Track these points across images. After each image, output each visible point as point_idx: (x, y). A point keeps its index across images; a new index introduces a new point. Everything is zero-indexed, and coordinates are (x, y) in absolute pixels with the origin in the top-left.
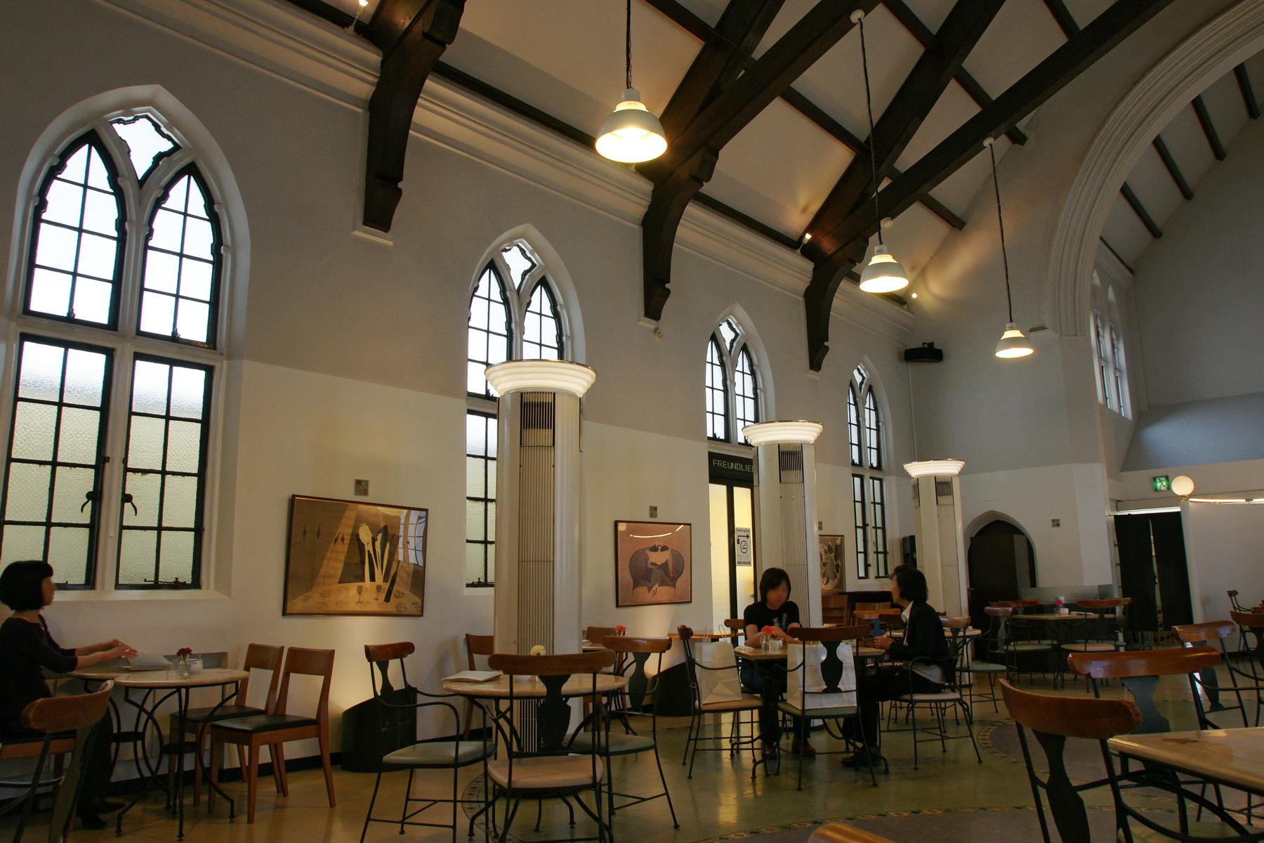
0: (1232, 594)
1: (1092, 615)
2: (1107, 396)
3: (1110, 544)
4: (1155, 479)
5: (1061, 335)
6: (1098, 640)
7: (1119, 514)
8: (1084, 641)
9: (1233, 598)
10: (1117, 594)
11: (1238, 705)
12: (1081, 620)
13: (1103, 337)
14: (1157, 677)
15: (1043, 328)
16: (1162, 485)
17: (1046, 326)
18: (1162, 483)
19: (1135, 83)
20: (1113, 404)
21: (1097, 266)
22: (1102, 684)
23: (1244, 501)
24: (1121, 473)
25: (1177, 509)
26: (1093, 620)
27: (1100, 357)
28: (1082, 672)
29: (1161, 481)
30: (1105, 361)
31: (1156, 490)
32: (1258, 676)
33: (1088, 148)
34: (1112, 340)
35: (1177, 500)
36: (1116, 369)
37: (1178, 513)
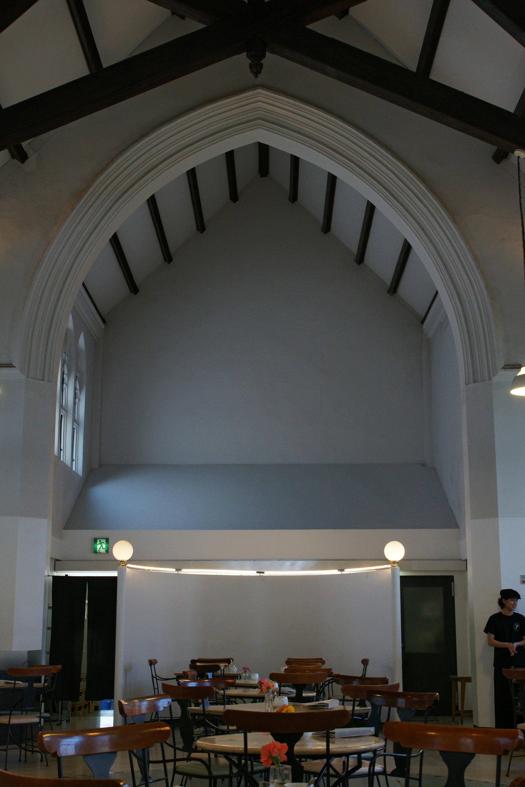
0: (152, 663)
1: (20, 684)
2: (62, 448)
3: (44, 607)
4: (95, 540)
5: (28, 377)
6: (22, 711)
7: (56, 574)
8: (9, 712)
9: (153, 666)
10: (44, 661)
11: (418, 777)
12: (9, 689)
13: (67, 385)
14: (115, 753)
15: (10, 366)
16: (101, 547)
17: (14, 365)
18: (102, 545)
19: (144, 135)
20: (66, 457)
21: (75, 313)
22: (20, 760)
23: (174, 570)
24: (64, 531)
25: (113, 574)
26: (21, 690)
27: (61, 406)
28: (49, 751)
29: (101, 543)
30: (65, 410)
31: (95, 552)
32: (177, 746)
33: (88, 187)
34: (75, 389)
35: (116, 564)
36: (75, 420)
37: (115, 579)
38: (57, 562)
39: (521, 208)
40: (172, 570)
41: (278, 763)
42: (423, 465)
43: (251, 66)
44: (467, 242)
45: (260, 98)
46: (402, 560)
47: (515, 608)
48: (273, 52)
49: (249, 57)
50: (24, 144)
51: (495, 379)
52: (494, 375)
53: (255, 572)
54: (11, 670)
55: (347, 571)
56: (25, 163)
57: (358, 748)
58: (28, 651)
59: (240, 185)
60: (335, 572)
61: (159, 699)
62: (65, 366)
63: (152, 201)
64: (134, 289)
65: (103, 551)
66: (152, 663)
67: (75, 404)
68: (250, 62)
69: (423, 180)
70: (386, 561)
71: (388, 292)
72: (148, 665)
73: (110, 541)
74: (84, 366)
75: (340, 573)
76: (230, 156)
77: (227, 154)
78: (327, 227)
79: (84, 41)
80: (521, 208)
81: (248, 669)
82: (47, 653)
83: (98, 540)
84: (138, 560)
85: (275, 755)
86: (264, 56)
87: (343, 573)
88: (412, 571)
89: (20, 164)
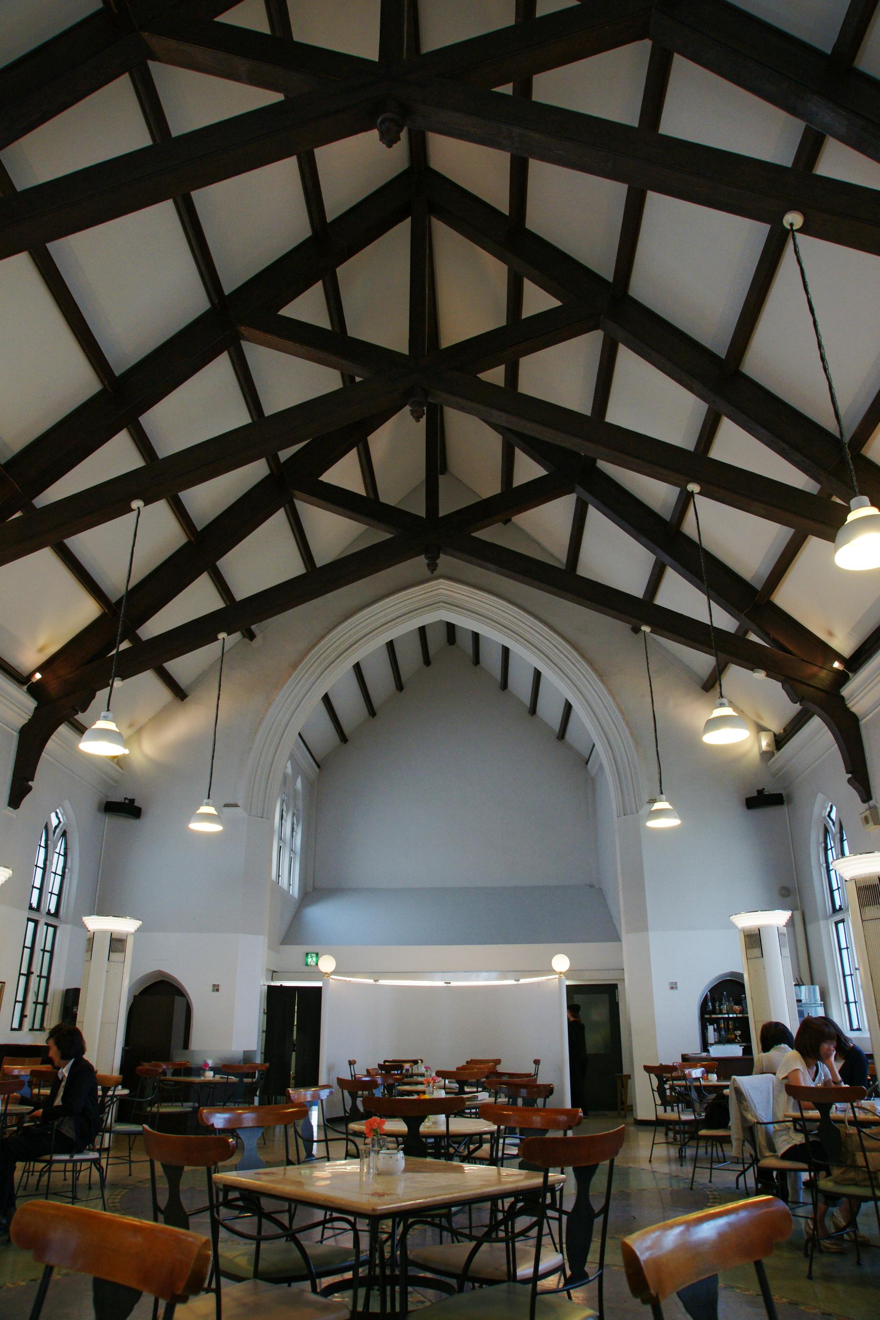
0: (351, 1063)
1: (233, 1079)
4: (307, 954)
7: (273, 984)
10: (259, 1059)
13: (286, 821)
16: (311, 960)
20: (284, 882)
26: (233, 1084)
29: (312, 957)
31: (307, 965)
34: (293, 824)
35: (320, 975)
38: (274, 973)
39: (648, 672)
40: (371, 981)
41: (377, 1134)
42: (591, 886)
43: (428, 565)
44: (614, 698)
45: (441, 586)
46: (568, 971)
47: (747, 1013)
48: (446, 554)
49: (427, 558)
50: (253, 627)
51: (640, 812)
52: (640, 809)
53: (443, 982)
54: (224, 1066)
55: (523, 981)
56: (253, 642)
57: (482, 1129)
58: (244, 1051)
59: (432, 652)
60: (512, 982)
61: (319, 1090)
62: (284, 805)
63: (357, 667)
64: (344, 739)
65: (313, 964)
66: (351, 1063)
67: (293, 836)
68: (428, 562)
69: (576, 648)
70: (552, 971)
71: (558, 738)
72: (348, 1064)
73: (319, 955)
74: (300, 804)
75: (516, 983)
76: (422, 630)
77: (420, 628)
78: (504, 685)
79: (299, 542)
80: (648, 672)
81: (429, 1068)
82: (262, 1053)
83: (309, 955)
84: (344, 972)
85: (375, 1128)
86: (438, 557)
87: (519, 983)
88: (581, 980)
89: (249, 642)
